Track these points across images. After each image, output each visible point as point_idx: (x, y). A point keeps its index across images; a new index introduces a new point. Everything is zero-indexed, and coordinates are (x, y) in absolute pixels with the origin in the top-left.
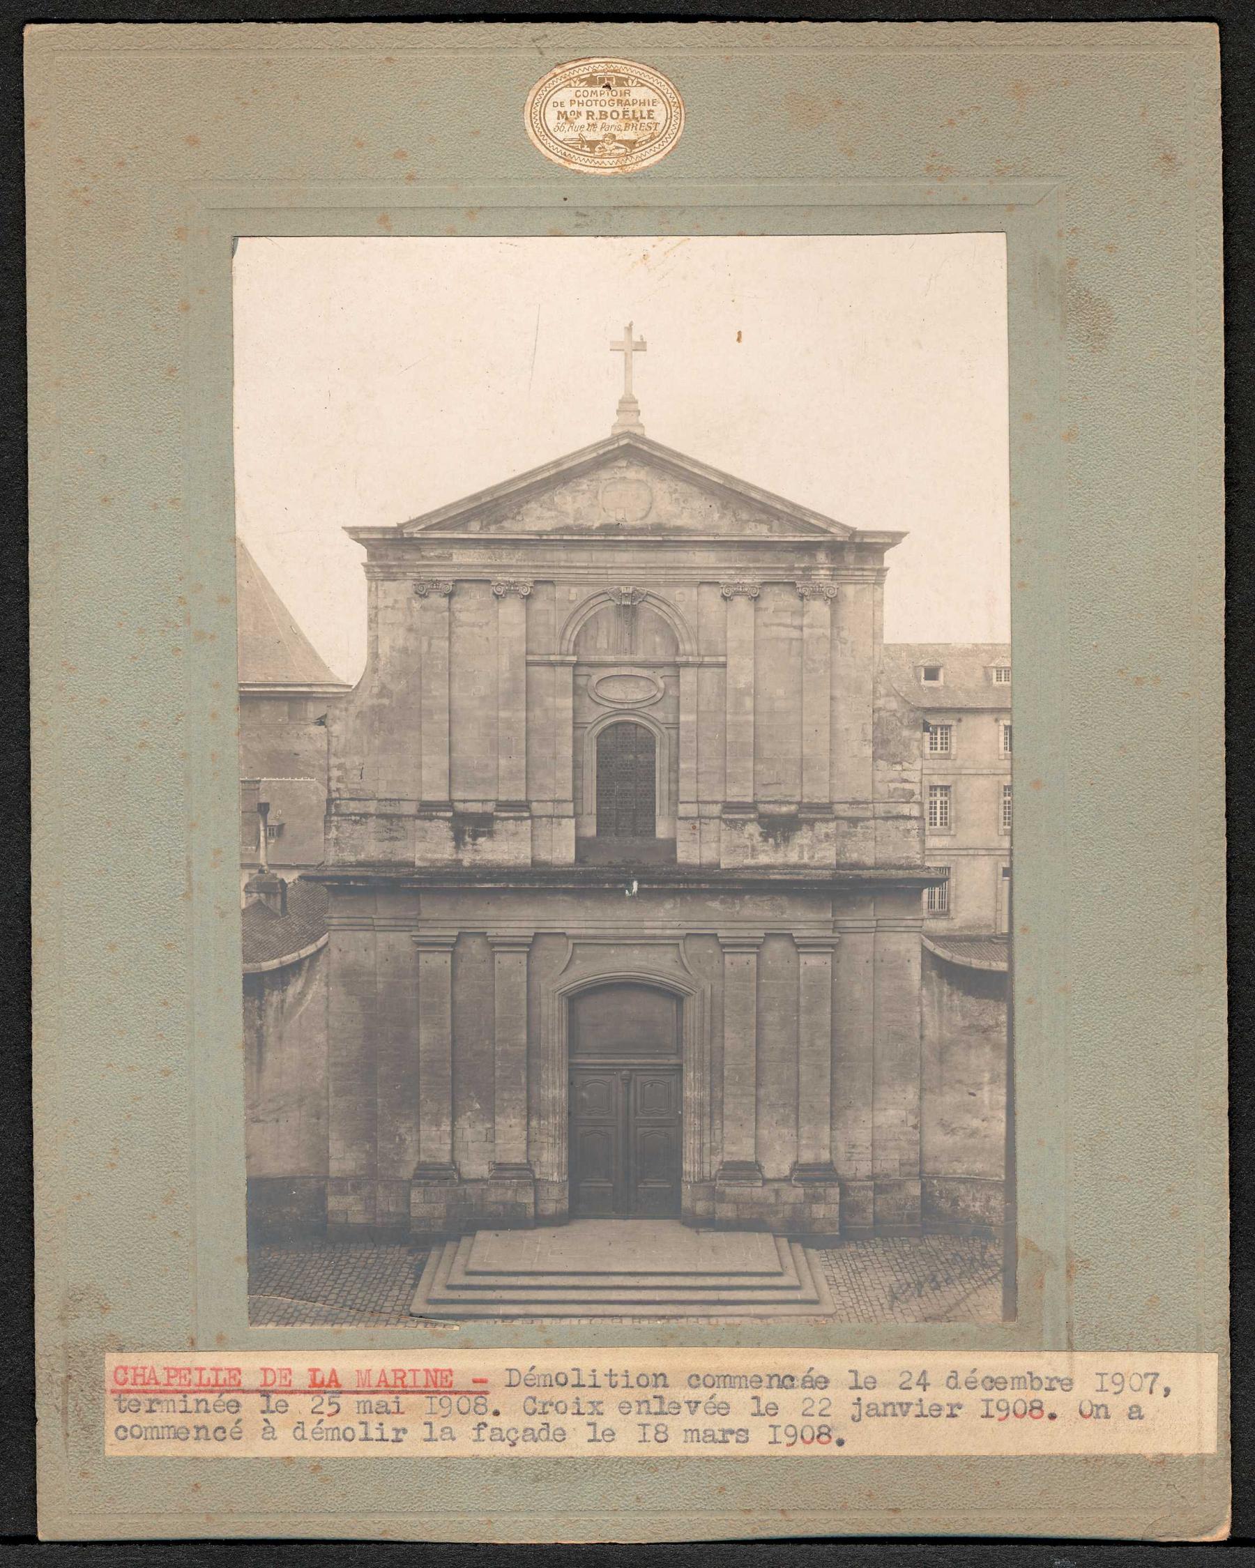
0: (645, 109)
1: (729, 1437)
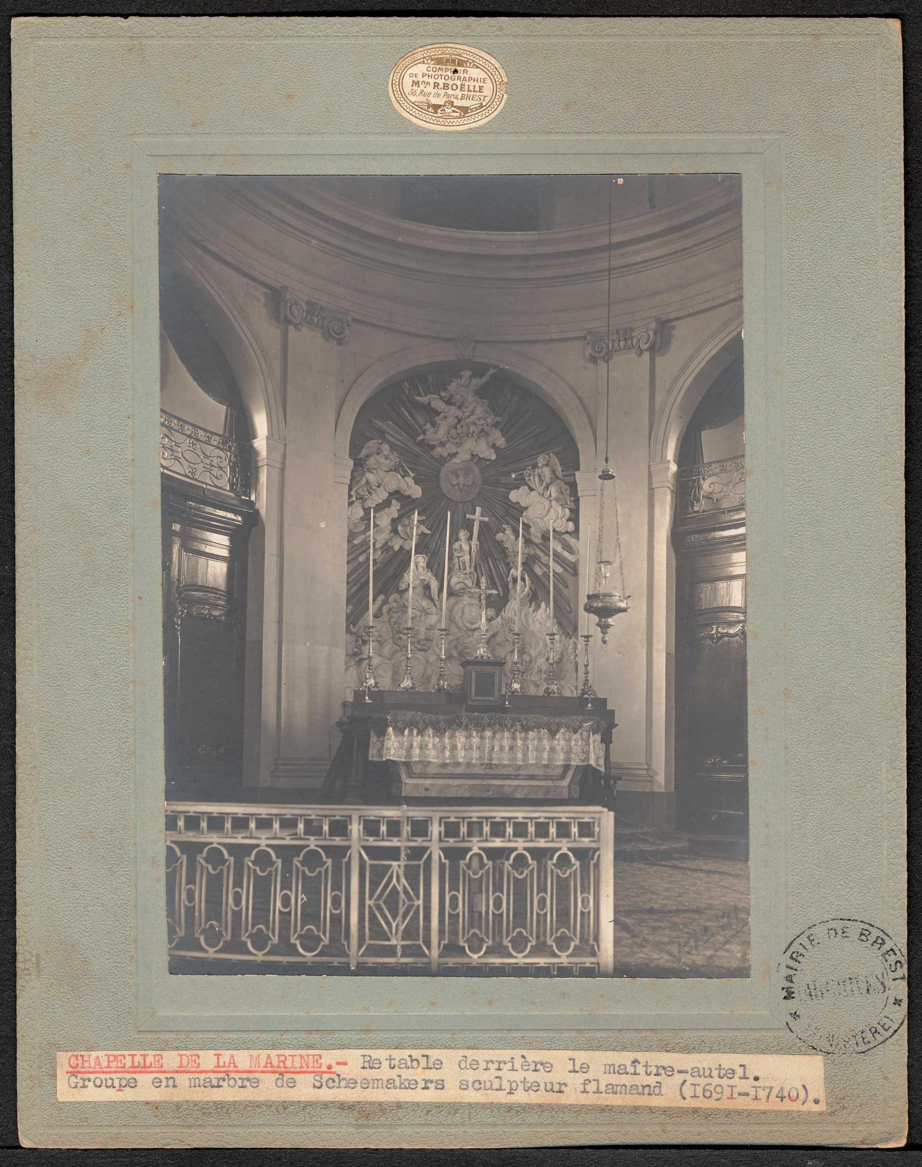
0: (477, 85)
1: (429, 1085)
